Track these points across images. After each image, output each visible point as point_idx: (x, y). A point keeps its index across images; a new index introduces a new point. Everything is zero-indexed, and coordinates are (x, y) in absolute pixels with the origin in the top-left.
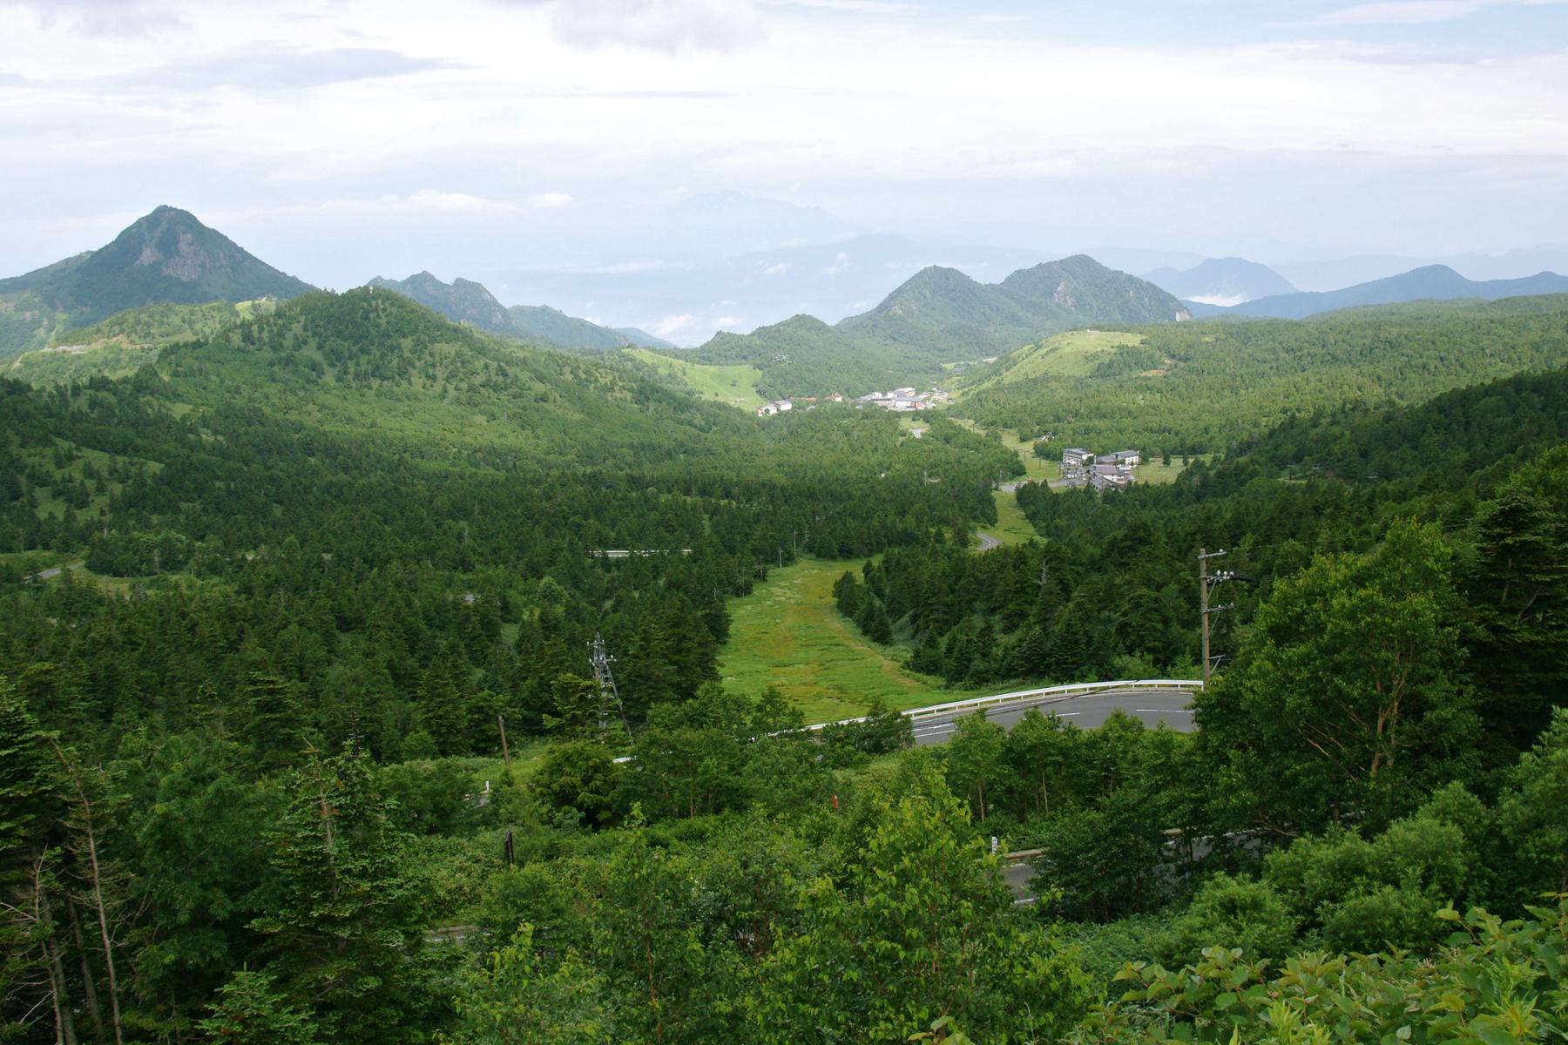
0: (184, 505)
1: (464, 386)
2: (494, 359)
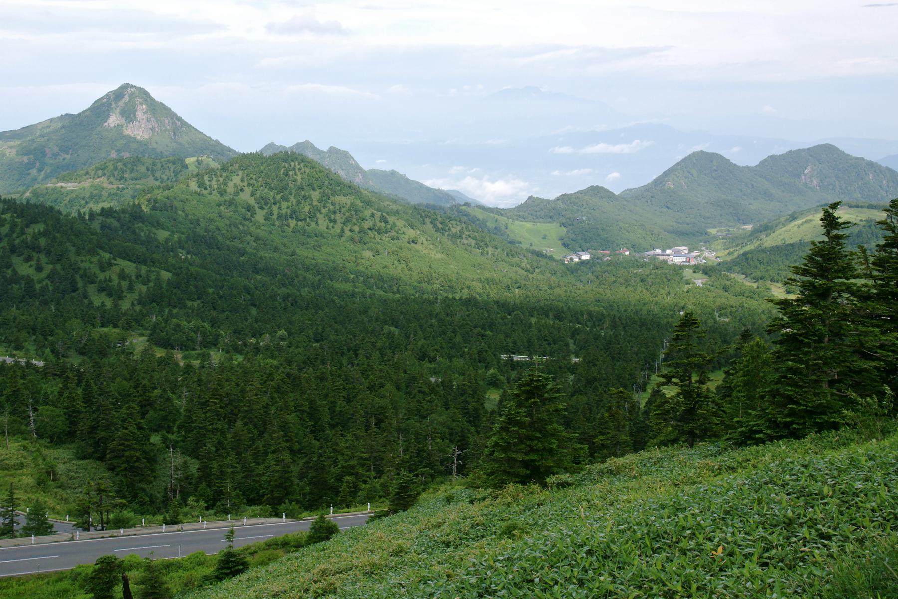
0: (189, 304)
1: (356, 228)
2: (378, 210)
